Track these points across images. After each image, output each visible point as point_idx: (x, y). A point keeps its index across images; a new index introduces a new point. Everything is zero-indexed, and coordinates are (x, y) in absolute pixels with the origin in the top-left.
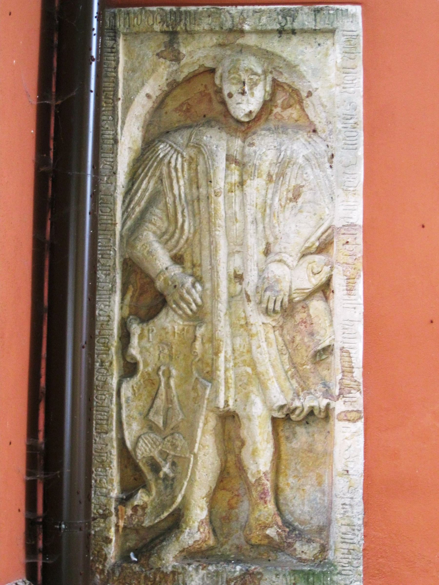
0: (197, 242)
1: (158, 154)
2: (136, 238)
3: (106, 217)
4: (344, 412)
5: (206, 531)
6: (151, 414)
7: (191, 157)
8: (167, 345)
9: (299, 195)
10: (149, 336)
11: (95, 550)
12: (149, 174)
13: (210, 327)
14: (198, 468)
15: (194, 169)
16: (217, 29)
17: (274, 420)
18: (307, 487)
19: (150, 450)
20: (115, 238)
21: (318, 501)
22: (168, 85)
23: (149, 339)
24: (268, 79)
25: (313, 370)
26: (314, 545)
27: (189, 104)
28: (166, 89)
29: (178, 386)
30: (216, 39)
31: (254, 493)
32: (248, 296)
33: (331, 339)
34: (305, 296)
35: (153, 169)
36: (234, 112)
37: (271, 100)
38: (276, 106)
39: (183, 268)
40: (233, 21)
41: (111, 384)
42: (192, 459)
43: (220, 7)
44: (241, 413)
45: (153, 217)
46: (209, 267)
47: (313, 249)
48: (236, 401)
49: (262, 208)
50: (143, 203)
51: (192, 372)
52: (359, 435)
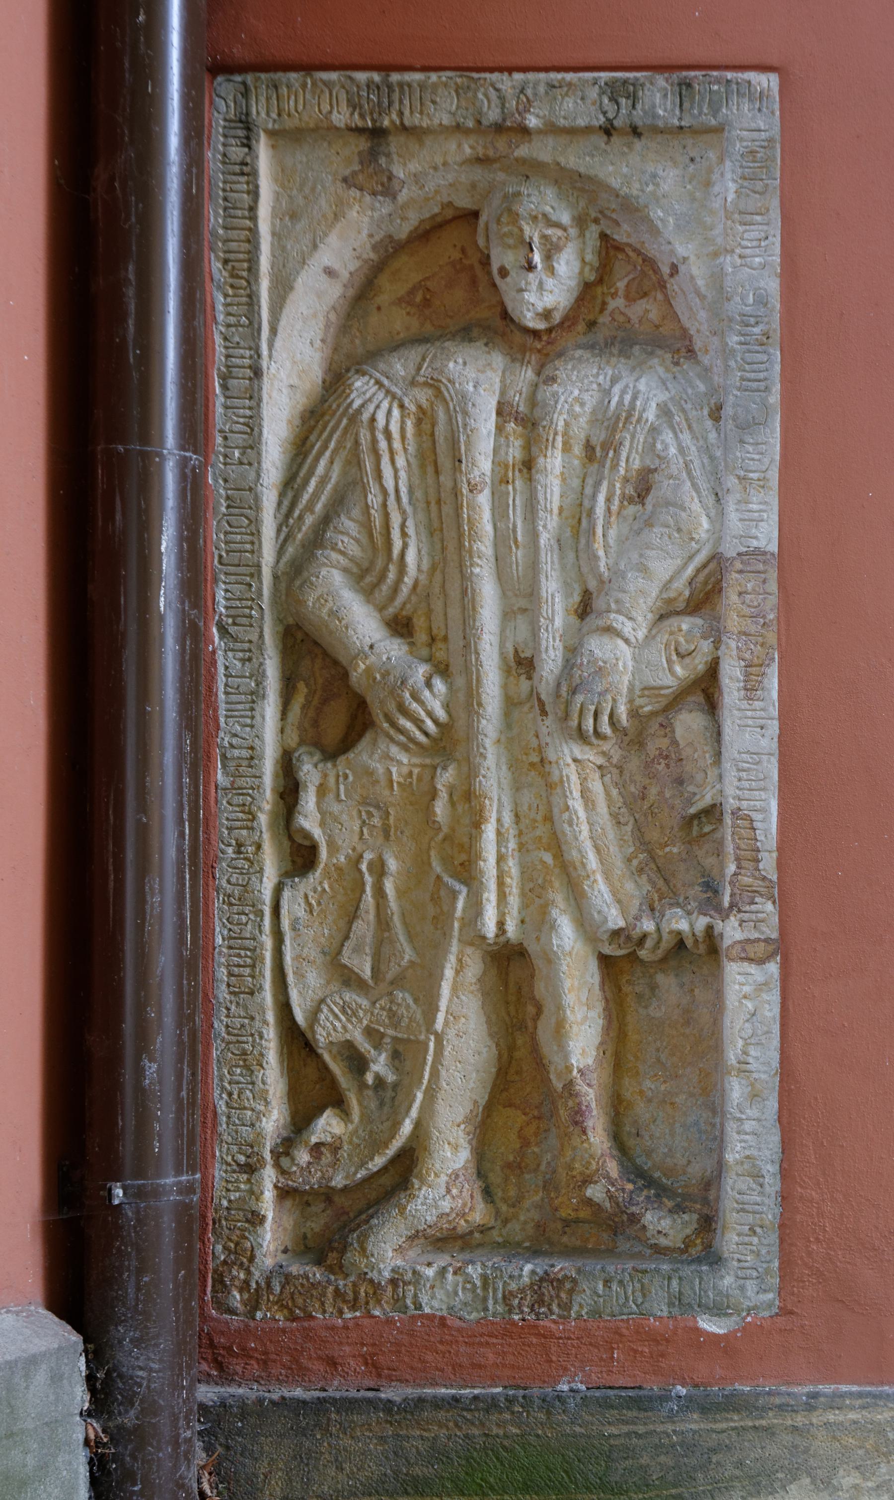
0: (437, 590)
1: (349, 401)
2: (305, 582)
3: (239, 537)
4: (740, 942)
5: (466, 1194)
6: (346, 952)
7: (420, 407)
8: (378, 807)
9: (648, 490)
10: (338, 789)
11: (230, 1240)
12: (332, 445)
13: (465, 769)
14: (445, 1063)
15: (429, 432)
16: (470, 124)
17: (605, 961)
18: (680, 1099)
19: (344, 1027)
20: (261, 583)
21: (703, 1127)
22: (374, 248)
23: (338, 795)
24: (588, 235)
25: (684, 856)
26: (686, 1217)
27: (428, 290)
28: (372, 256)
29: (401, 893)
30: (471, 147)
31: (561, 1112)
32: (541, 703)
33: (714, 791)
34: (664, 702)
35: (338, 433)
36: (513, 309)
37: (600, 281)
38: (614, 295)
39: (412, 644)
40: (503, 106)
41: (259, 891)
42: (432, 1045)
43: (475, 75)
44: (532, 948)
45: (341, 537)
46: (461, 643)
47: (681, 605)
48: (522, 922)
49: (574, 517)
50: (319, 507)
51: (430, 864)
52: (771, 990)
